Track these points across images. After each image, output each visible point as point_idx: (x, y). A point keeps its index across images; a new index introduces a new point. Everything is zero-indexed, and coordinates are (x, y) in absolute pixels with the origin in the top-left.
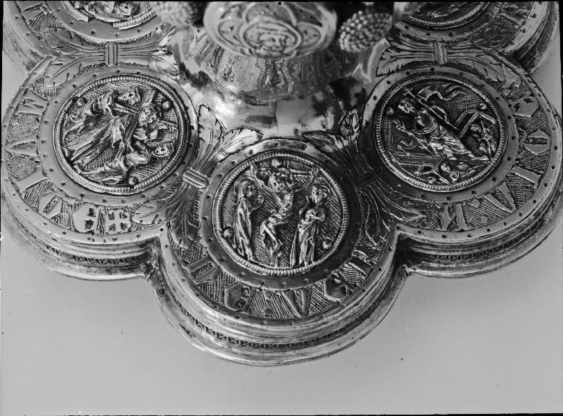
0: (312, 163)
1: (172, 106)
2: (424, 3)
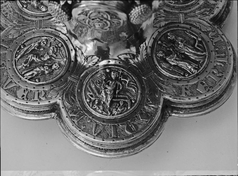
0: (67, 57)
2: (161, 2)
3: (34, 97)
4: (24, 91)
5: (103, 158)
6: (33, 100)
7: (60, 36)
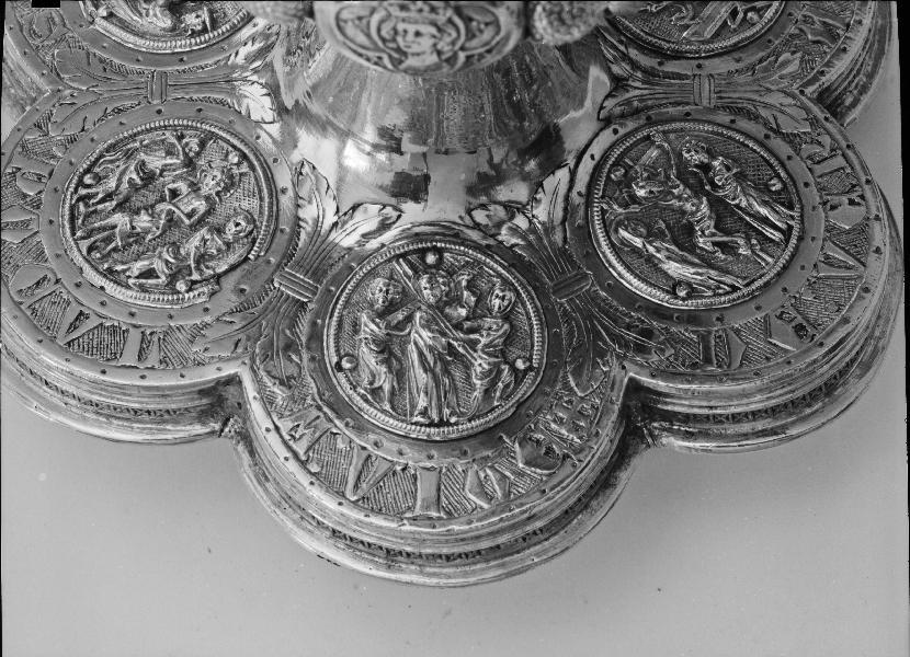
1: (439, 252)
3: (836, 170)
4: (833, 208)
5: (124, 446)
6: (849, 170)
7: (583, 191)
